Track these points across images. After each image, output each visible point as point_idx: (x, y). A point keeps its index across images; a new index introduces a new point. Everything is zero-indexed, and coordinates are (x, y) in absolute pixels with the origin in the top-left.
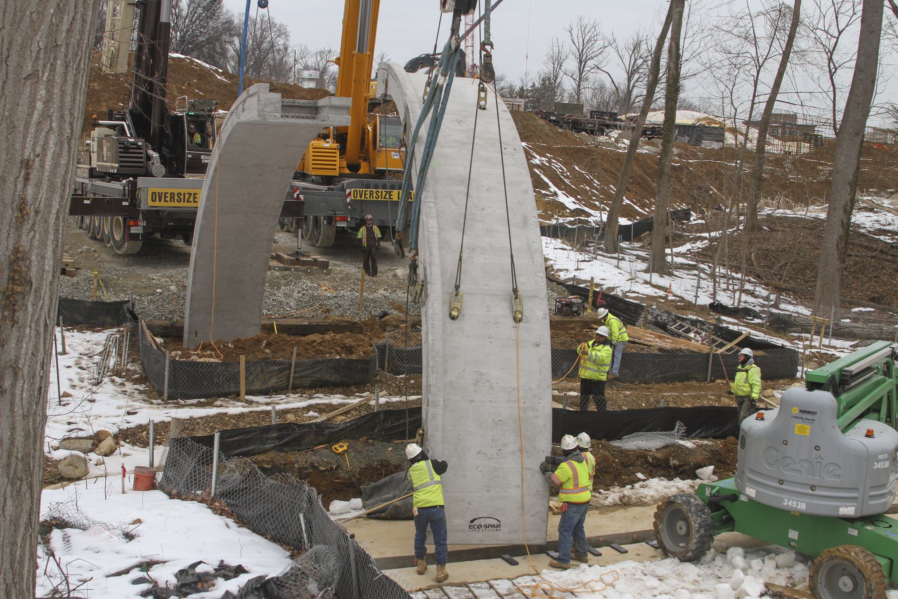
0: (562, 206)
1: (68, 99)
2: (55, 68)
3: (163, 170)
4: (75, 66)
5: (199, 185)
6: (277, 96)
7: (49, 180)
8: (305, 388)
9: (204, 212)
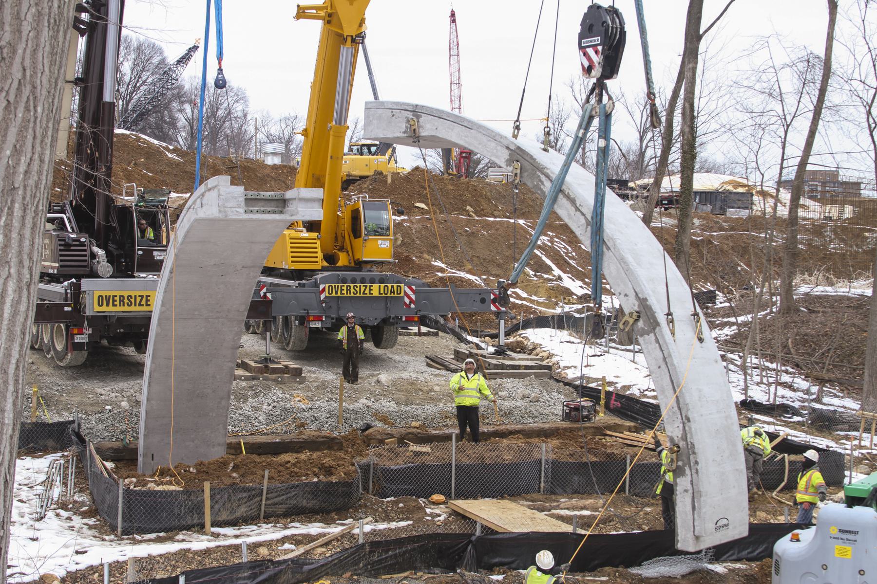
0: (568, 292)
1: (27, 243)
2: (13, 212)
3: (110, 269)
4: (33, 209)
5: (153, 286)
7: (8, 329)
8: (278, 516)
9: (160, 319)
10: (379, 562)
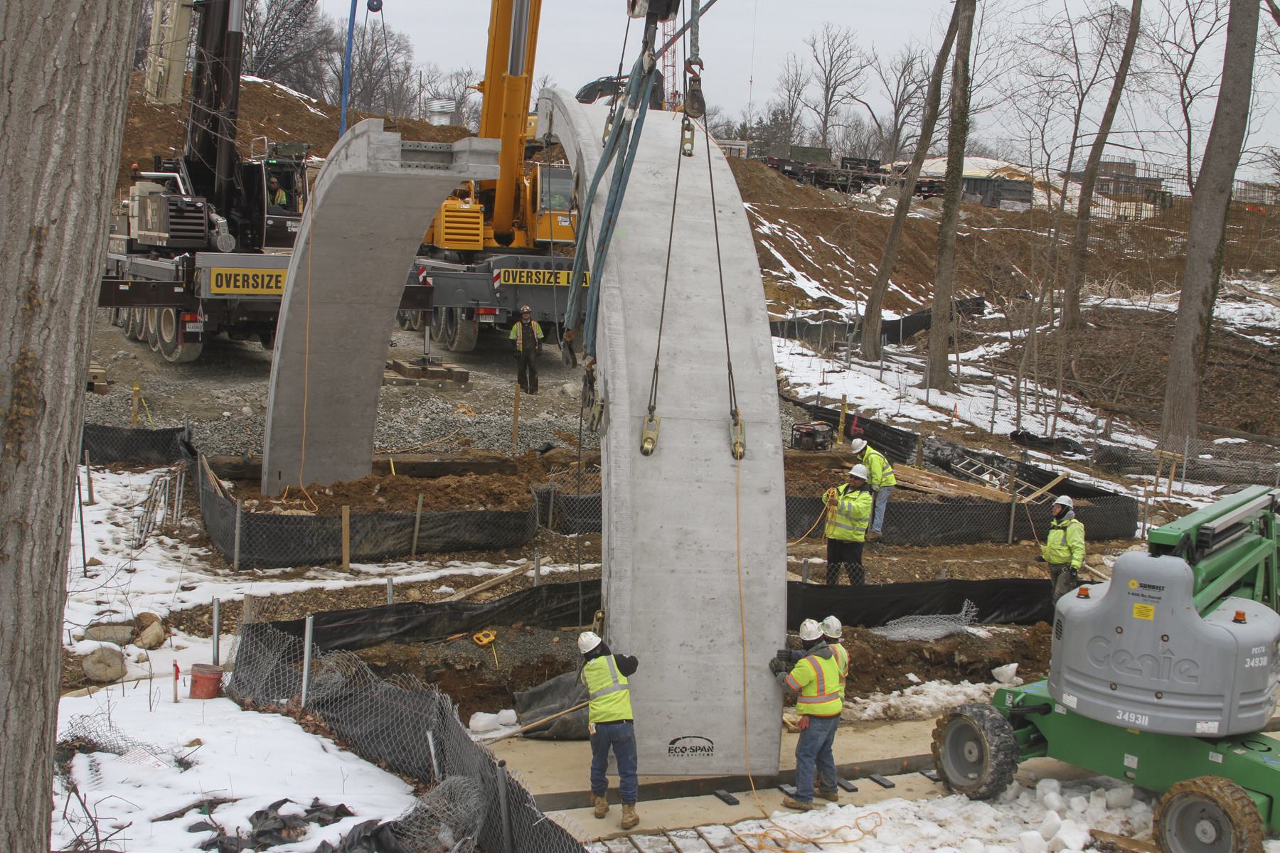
0: (801, 294)
1: (97, 141)
2: (78, 97)
3: (232, 242)
4: (107, 95)
5: (284, 263)
6: (395, 137)
7: (70, 257)
8: (434, 552)
9: (291, 302)
10: (560, 610)
